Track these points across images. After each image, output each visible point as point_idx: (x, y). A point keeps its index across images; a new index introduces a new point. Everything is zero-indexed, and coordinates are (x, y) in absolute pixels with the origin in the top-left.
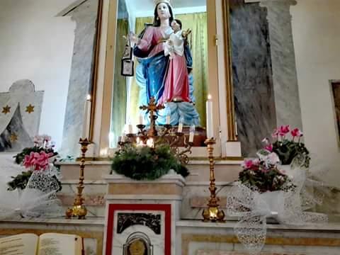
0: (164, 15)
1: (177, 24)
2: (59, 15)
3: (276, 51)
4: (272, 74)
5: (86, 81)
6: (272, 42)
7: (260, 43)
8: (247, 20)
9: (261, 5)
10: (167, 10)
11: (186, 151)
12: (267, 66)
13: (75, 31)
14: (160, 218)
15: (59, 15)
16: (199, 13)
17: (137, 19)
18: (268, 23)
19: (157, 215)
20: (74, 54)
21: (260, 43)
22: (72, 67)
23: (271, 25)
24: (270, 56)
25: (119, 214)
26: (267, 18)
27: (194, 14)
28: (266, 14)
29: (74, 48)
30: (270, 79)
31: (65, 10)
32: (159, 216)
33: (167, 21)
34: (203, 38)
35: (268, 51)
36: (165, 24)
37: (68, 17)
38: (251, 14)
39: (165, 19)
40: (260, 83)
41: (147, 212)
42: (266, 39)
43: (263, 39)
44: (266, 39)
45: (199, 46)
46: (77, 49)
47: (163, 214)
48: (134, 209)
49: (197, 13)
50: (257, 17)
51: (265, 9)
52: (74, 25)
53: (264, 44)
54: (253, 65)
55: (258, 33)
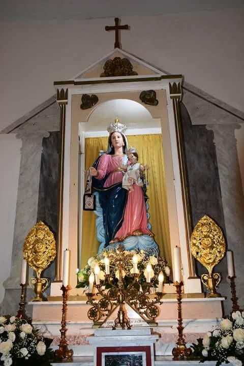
0: (118, 145)
1: (134, 157)
2: (3, 132)
3: (224, 175)
4: (221, 198)
5: (34, 204)
6: (219, 165)
7: (209, 166)
8: (195, 143)
9: (208, 128)
10: (121, 139)
11: (156, 302)
12: (216, 189)
13: (21, 149)
14: (141, 359)
15: (3, 132)
16: (149, 135)
17: (86, 139)
18: (215, 146)
19: (139, 357)
20: (21, 174)
21: (209, 166)
22: (19, 189)
23: (218, 149)
24: (218, 179)
25: (106, 356)
26: (214, 141)
27: (143, 136)
28: (213, 138)
29: (21, 168)
30: (220, 202)
31: (10, 127)
32: (141, 357)
33: (121, 149)
34: (153, 154)
35: (217, 175)
36: (120, 152)
37: (13, 135)
38: (198, 136)
39: (120, 147)
40: (210, 207)
41: (121, 353)
42: (214, 162)
43: (211, 162)
44: (214, 162)
45: (151, 175)
46: (24, 169)
47: (144, 354)
48: (118, 351)
49: (146, 135)
50: (204, 140)
51: (212, 132)
52: (19, 143)
53: (212, 167)
54: (203, 189)
55: (206, 156)
